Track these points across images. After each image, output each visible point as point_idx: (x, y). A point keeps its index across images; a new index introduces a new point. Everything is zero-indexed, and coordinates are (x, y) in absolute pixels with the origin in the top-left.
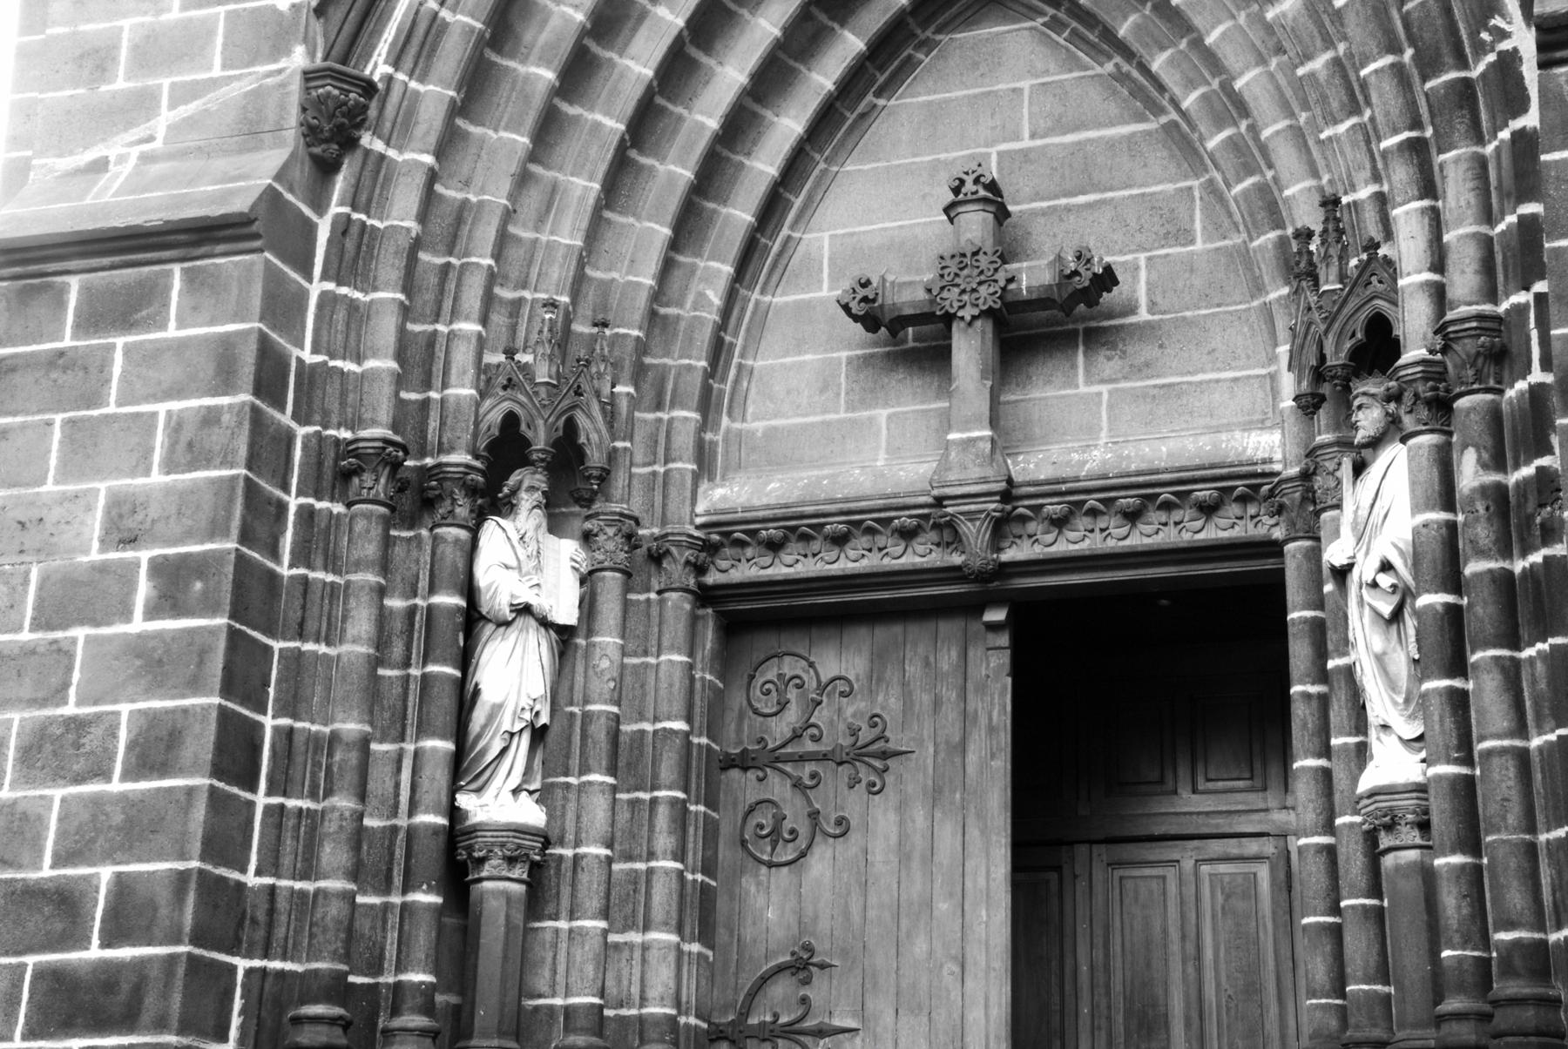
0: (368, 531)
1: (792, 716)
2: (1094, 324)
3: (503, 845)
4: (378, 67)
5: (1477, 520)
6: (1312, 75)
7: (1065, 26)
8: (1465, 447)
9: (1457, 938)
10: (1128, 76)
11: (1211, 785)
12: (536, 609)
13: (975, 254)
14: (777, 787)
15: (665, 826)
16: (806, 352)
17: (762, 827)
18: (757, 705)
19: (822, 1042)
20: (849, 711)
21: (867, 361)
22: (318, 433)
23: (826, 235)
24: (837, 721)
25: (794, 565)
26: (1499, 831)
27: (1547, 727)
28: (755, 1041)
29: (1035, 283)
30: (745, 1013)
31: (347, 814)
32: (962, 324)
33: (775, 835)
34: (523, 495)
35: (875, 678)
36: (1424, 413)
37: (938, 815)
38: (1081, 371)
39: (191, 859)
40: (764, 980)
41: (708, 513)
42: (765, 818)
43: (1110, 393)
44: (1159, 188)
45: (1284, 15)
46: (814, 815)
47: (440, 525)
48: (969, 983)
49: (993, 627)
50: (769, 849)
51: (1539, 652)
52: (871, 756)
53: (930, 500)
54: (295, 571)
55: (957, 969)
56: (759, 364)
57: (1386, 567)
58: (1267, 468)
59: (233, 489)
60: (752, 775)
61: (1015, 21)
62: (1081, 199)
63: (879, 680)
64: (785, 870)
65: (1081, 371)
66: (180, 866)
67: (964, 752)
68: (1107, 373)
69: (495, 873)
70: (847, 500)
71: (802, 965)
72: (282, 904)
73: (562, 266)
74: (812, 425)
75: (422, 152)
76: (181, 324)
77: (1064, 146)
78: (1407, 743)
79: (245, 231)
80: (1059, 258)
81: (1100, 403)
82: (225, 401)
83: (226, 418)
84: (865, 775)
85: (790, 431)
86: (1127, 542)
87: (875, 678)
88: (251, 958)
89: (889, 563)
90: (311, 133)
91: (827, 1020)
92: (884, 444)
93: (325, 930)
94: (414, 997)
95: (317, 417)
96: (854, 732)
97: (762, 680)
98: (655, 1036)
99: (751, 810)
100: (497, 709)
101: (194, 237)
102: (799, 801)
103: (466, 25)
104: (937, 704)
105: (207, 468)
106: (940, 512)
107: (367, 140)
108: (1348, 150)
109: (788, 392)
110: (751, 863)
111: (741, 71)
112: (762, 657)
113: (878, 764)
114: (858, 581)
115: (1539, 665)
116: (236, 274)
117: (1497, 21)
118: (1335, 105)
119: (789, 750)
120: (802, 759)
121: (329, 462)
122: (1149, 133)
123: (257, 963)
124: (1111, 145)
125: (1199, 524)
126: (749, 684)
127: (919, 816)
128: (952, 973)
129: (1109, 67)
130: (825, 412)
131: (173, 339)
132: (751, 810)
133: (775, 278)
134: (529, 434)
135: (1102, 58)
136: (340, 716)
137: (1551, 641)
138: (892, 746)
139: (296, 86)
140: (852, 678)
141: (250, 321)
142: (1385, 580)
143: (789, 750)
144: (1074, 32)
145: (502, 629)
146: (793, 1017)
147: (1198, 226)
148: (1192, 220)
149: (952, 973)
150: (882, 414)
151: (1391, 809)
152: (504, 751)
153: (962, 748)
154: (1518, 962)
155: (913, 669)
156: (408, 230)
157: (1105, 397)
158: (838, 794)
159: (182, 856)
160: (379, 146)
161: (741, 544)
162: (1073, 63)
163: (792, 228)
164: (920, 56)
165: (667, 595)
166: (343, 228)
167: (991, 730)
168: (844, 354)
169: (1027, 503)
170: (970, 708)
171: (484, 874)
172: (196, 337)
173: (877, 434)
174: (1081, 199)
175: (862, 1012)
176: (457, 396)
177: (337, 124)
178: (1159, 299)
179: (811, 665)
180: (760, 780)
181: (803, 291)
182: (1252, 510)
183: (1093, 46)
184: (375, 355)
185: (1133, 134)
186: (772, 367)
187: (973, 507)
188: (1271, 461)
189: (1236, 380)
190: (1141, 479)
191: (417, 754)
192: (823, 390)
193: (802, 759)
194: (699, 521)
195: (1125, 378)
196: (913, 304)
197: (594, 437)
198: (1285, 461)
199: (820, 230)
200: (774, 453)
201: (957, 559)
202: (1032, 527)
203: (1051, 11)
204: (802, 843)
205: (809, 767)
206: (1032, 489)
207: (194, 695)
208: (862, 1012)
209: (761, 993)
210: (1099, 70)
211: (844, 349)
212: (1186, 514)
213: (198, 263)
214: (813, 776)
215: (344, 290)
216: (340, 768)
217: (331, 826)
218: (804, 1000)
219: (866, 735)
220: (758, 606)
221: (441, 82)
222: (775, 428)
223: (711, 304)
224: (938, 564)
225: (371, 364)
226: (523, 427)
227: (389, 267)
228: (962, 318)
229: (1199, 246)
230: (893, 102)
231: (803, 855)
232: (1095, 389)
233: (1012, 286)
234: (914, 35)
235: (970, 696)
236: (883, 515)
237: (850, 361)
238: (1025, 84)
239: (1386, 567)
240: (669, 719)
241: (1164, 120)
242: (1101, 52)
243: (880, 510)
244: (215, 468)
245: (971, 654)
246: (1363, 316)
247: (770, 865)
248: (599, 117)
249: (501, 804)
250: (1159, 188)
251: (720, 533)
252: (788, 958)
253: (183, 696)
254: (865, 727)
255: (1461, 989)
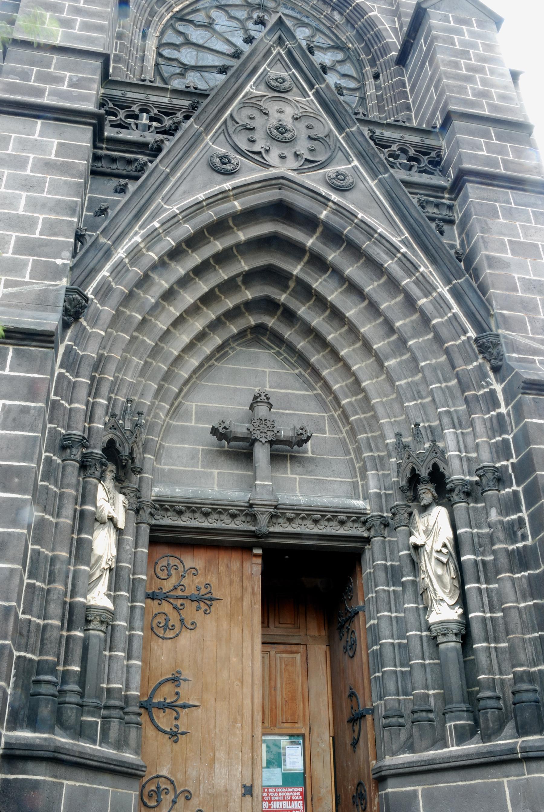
0: (73, 473)
1: (173, 581)
2: (293, 454)
3: (101, 616)
4: (89, 292)
5: (499, 531)
6: (401, 385)
7: (282, 355)
8: (491, 507)
9: (487, 671)
10: (304, 376)
11: (280, 625)
12: (115, 520)
13: (265, 420)
14: (166, 607)
15: (139, 618)
16: (186, 444)
17: (160, 623)
18: (158, 575)
19: (184, 710)
20: (197, 581)
21: (210, 451)
22: (55, 428)
23: (194, 404)
24: (192, 584)
25: (186, 521)
26: (515, 634)
27: (528, 600)
28: (156, 709)
29: (286, 435)
30: (151, 698)
31: (61, 592)
32: (261, 444)
33: (166, 627)
34: (108, 473)
35: (207, 569)
36: (462, 496)
37: (232, 624)
38: (289, 469)
39: (12, 601)
40: (160, 684)
41: (156, 496)
42: (161, 619)
43: (300, 478)
44: (314, 414)
45: (391, 365)
46: (182, 621)
47: (89, 477)
48: (244, 690)
49: (256, 556)
50: (163, 632)
51: (523, 576)
52: (205, 600)
53: (246, 505)
54: (43, 483)
55: (240, 684)
56: (167, 445)
57: (445, 546)
58: (365, 511)
59: (35, 441)
60: (156, 602)
61: (263, 349)
62: (287, 412)
63: (208, 571)
64: (170, 641)
65: (289, 469)
66: (6, 604)
67: (242, 601)
68: (298, 471)
69: (95, 627)
70: (214, 500)
71: (175, 680)
72: (33, 629)
73: (127, 388)
74: (188, 471)
75: (101, 330)
76: (11, 370)
77: (281, 393)
78: (449, 606)
79: (49, 339)
80: (295, 428)
81: (296, 481)
82: (32, 404)
83: (32, 412)
84: (203, 606)
85: (180, 471)
86: (313, 531)
87: (207, 569)
88: (20, 651)
89: (224, 526)
90: (66, 311)
91: (187, 702)
92: (216, 482)
93: (51, 642)
94: (74, 677)
95: (55, 421)
96: (198, 589)
97: (161, 565)
98: (134, 703)
99: (156, 615)
100: (100, 557)
101: (24, 336)
102: (175, 613)
103: (122, 290)
104: (231, 582)
105: (22, 430)
106: (250, 509)
107: (82, 320)
108: (414, 411)
109: (178, 457)
110: (155, 637)
111: (188, 338)
112: (161, 556)
113: (208, 602)
114: (212, 531)
115: (523, 580)
116: (39, 355)
117: (488, 379)
118: (409, 396)
119: (171, 593)
120: (177, 598)
121: (58, 441)
122: (310, 395)
123: (22, 654)
124: (297, 396)
125: (338, 527)
126: (155, 566)
127: (225, 625)
128: (238, 685)
129: (297, 371)
130: (193, 467)
131: (8, 375)
132: (156, 615)
133: (174, 415)
134: (120, 449)
135: (294, 368)
136: (59, 549)
137: (529, 572)
138: (214, 596)
139: (63, 292)
140: (198, 569)
141: (46, 375)
142: (445, 550)
143: (171, 593)
144: (285, 357)
145: (102, 525)
146: (172, 700)
147: (327, 428)
148: (325, 426)
149: (238, 685)
150: (216, 472)
151: (447, 628)
152: (101, 576)
153: (241, 599)
154: (525, 678)
155: (222, 568)
156: (94, 357)
157: (298, 480)
158: (190, 611)
159: (7, 599)
160: (85, 323)
161: (167, 510)
162: (283, 368)
163: (182, 398)
164: (230, 352)
165: (141, 525)
166: (69, 350)
167: (253, 593)
168: (201, 447)
169: (281, 511)
170: (244, 585)
171: (91, 627)
172: (19, 376)
173: (214, 478)
174: (287, 412)
175: (201, 700)
176: (98, 427)
177: (74, 311)
178: (315, 450)
179: (181, 562)
180: (159, 604)
181: (184, 422)
182: (356, 525)
183: (292, 363)
184: (78, 402)
185: (304, 395)
186: (172, 447)
187: (264, 510)
188: (366, 509)
189: (341, 481)
190: (323, 509)
191: (75, 571)
192: (192, 459)
193: (177, 598)
194: (153, 498)
195: (305, 474)
196: (241, 433)
197: (138, 455)
198: (371, 510)
199: (191, 402)
200: (171, 478)
201: (253, 529)
202: (280, 520)
203: (277, 349)
204: (177, 631)
205: (180, 602)
206: (284, 507)
207: (14, 527)
208: (201, 700)
209: (159, 690)
210: (292, 371)
211: (200, 445)
212: (334, 523)
213: (21, 347)
214: (181, 605)
215: (67, 374)
216: (59, 571)
217: (54, 596)
218: (177, 693)
219: (203, 591)
220: (170, 535)
221: (110, 307)
222: (173, 470)
223: (161, 418)
224: (246, 529)
225: (76, 405)
226: (118, 445)
227: (86, 369)
228: (261, 441)
229: (327, 435)
230: (219, 365)
231: (177, 635)
232: (294, 476)
233: (278, 434)
234: (230, 344)
235: (244, 581)
236: (226, 507)
237: (203, 450)
238: (267, 370)
239: (445, 546)
240: (141, 574)
241: (315, 392)
242: (295, 366)
243: (226, 505)
244: (26, 431)
245: (244, 565)
246: (432, 463)
247: (163, 638)
248: (145, 338)
249: (99, 597)
250: (314, 414)
251: (159, 505)
252: (171, 676)
253: (8, 528)
254: (203, 588)
255: (489, 688)
